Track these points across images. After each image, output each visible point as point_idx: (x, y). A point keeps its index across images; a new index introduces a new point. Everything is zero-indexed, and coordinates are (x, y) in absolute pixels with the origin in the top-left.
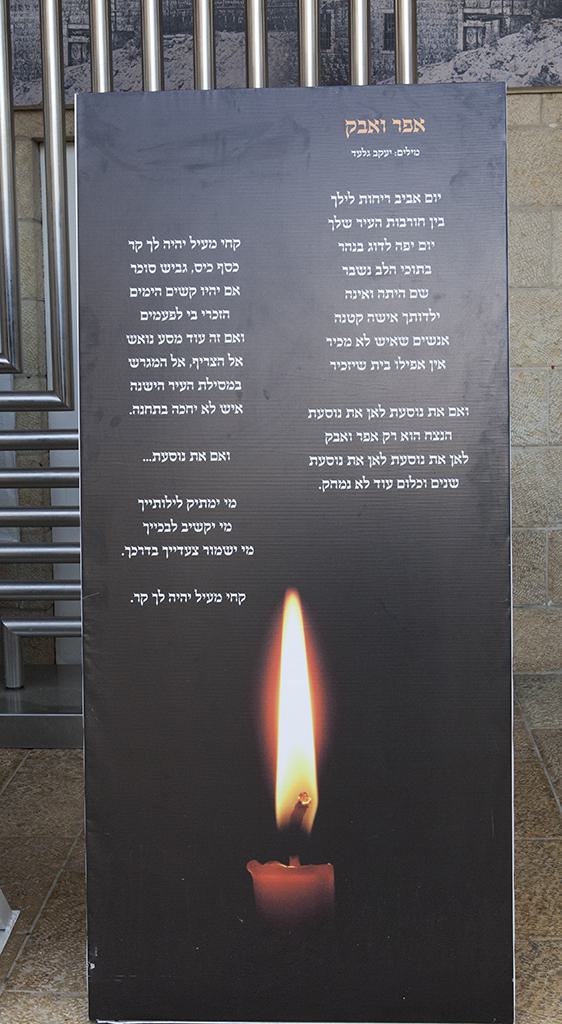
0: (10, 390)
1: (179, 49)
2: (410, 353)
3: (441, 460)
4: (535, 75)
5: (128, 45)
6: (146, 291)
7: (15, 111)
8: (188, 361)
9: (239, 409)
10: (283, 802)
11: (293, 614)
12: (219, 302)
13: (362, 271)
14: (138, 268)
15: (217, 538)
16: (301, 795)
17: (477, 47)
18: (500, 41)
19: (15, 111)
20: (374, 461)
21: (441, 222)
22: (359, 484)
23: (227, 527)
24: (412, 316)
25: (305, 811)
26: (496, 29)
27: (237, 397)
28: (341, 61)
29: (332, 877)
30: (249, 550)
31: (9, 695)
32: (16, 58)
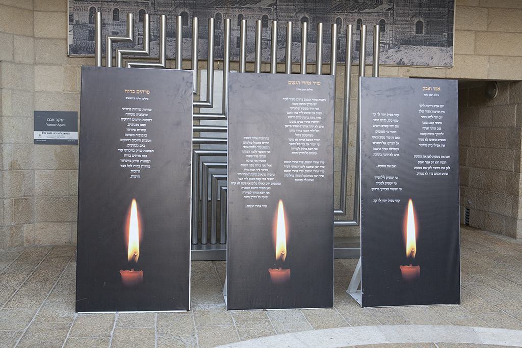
2: (437, 143)
3: (444, 168)
6: (377, 126)
8: (387, 143)
9: (398, 155)
10: (408, 251)
11: (410, 203)
12: (393, 129)
13: (427, 123)
14: (375, 120)
15: (393, 186)
18: (389, 51)
20: (429, 168)
21: (444, 112)
22: (425, 174)
23: (395, 183)
24: (437, 134)
26: (388, 47)
27: (398, 152)
30: (401, 189)
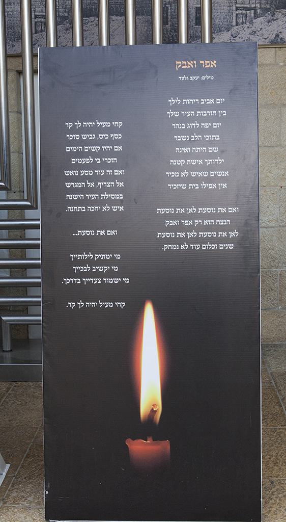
0: (5, 199)
1: (91, 25)
2: (209, 180)
3: (225, 234)
4: (272, 38)
5: (65, 23)
6: (75, 149)
7: (8, 56)
8: (96, 184)
9: (122, 208)
10: (144, 409)
11: (149, 313)
12: (112, 154)
13: (184, 138)
14: (70, 137)
15: (110, 274)
16: (153, 405)
17: (243, 24)
18: (254, 21)
19: (8, 56)
20: (190, 235)
21: (225, 113)
22: (183, 247)
23: (116, 269)
24: (210, 161)
25: (155, 414)
26: (253, 15)
27: (121, 202)
28: (173, 31)
29: (169, 447)
30: (127, 280)
31: (5, 354)
32: (8, 29)
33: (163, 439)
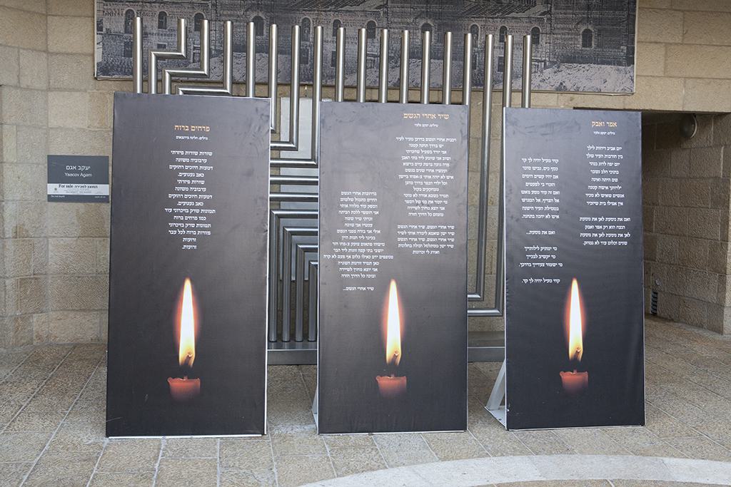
2: (612, 199)
3: (622, 235)
6: (528, 176)
8: (542, 200)
9: (558, 217)
10: (571, 351)
11: (575, 285)
12: (551, 180)
13: (597, 172)
14: (525, 168)
15: (551, 260)
18: (544, 71)
20: (601, 235)
21: (621, 157)
22: (596, 243)
23: (554, 257)
24: (612, 188)
26: (543, 66)
27: (557, 213)
30: (561, 265)
33: (401, 376)
